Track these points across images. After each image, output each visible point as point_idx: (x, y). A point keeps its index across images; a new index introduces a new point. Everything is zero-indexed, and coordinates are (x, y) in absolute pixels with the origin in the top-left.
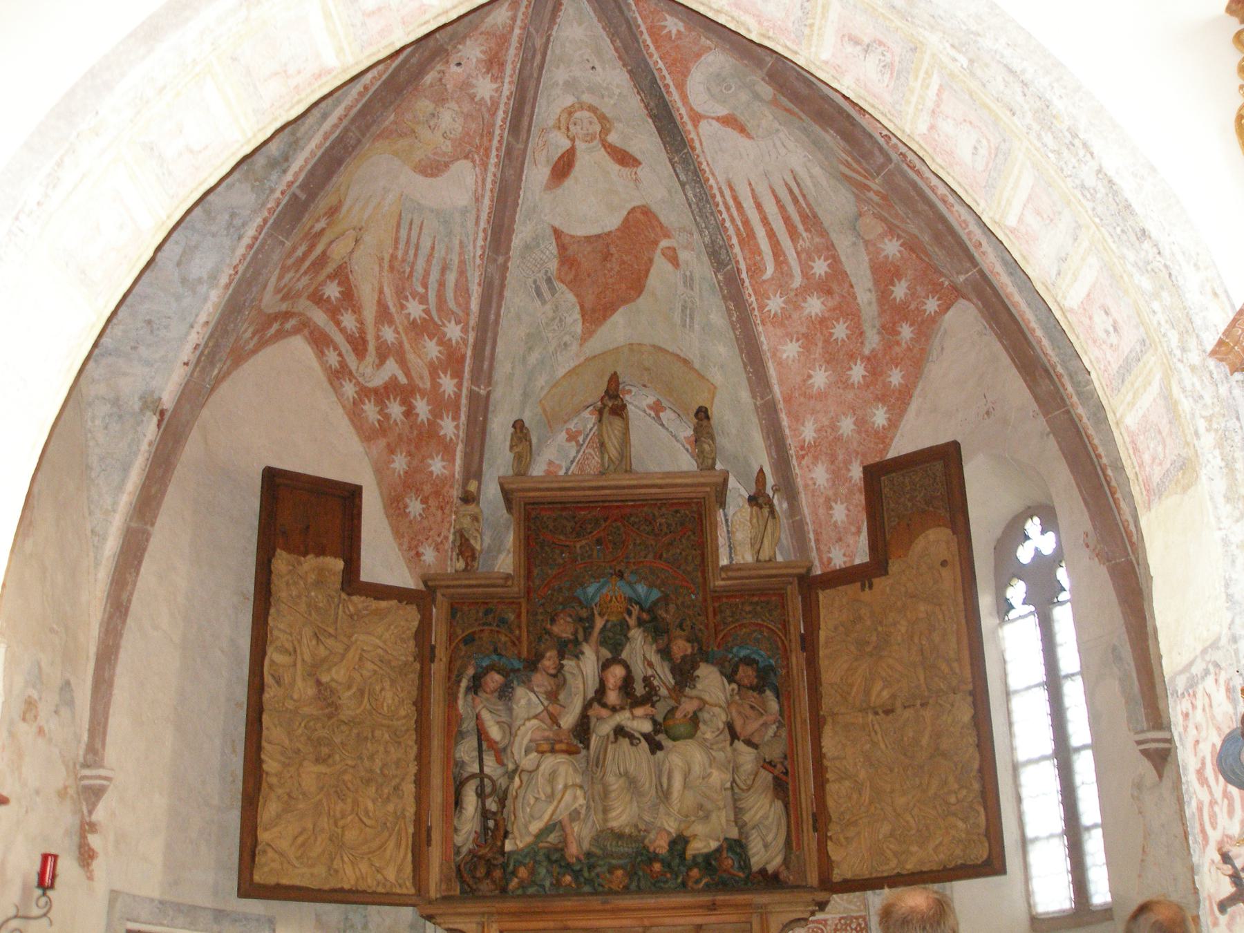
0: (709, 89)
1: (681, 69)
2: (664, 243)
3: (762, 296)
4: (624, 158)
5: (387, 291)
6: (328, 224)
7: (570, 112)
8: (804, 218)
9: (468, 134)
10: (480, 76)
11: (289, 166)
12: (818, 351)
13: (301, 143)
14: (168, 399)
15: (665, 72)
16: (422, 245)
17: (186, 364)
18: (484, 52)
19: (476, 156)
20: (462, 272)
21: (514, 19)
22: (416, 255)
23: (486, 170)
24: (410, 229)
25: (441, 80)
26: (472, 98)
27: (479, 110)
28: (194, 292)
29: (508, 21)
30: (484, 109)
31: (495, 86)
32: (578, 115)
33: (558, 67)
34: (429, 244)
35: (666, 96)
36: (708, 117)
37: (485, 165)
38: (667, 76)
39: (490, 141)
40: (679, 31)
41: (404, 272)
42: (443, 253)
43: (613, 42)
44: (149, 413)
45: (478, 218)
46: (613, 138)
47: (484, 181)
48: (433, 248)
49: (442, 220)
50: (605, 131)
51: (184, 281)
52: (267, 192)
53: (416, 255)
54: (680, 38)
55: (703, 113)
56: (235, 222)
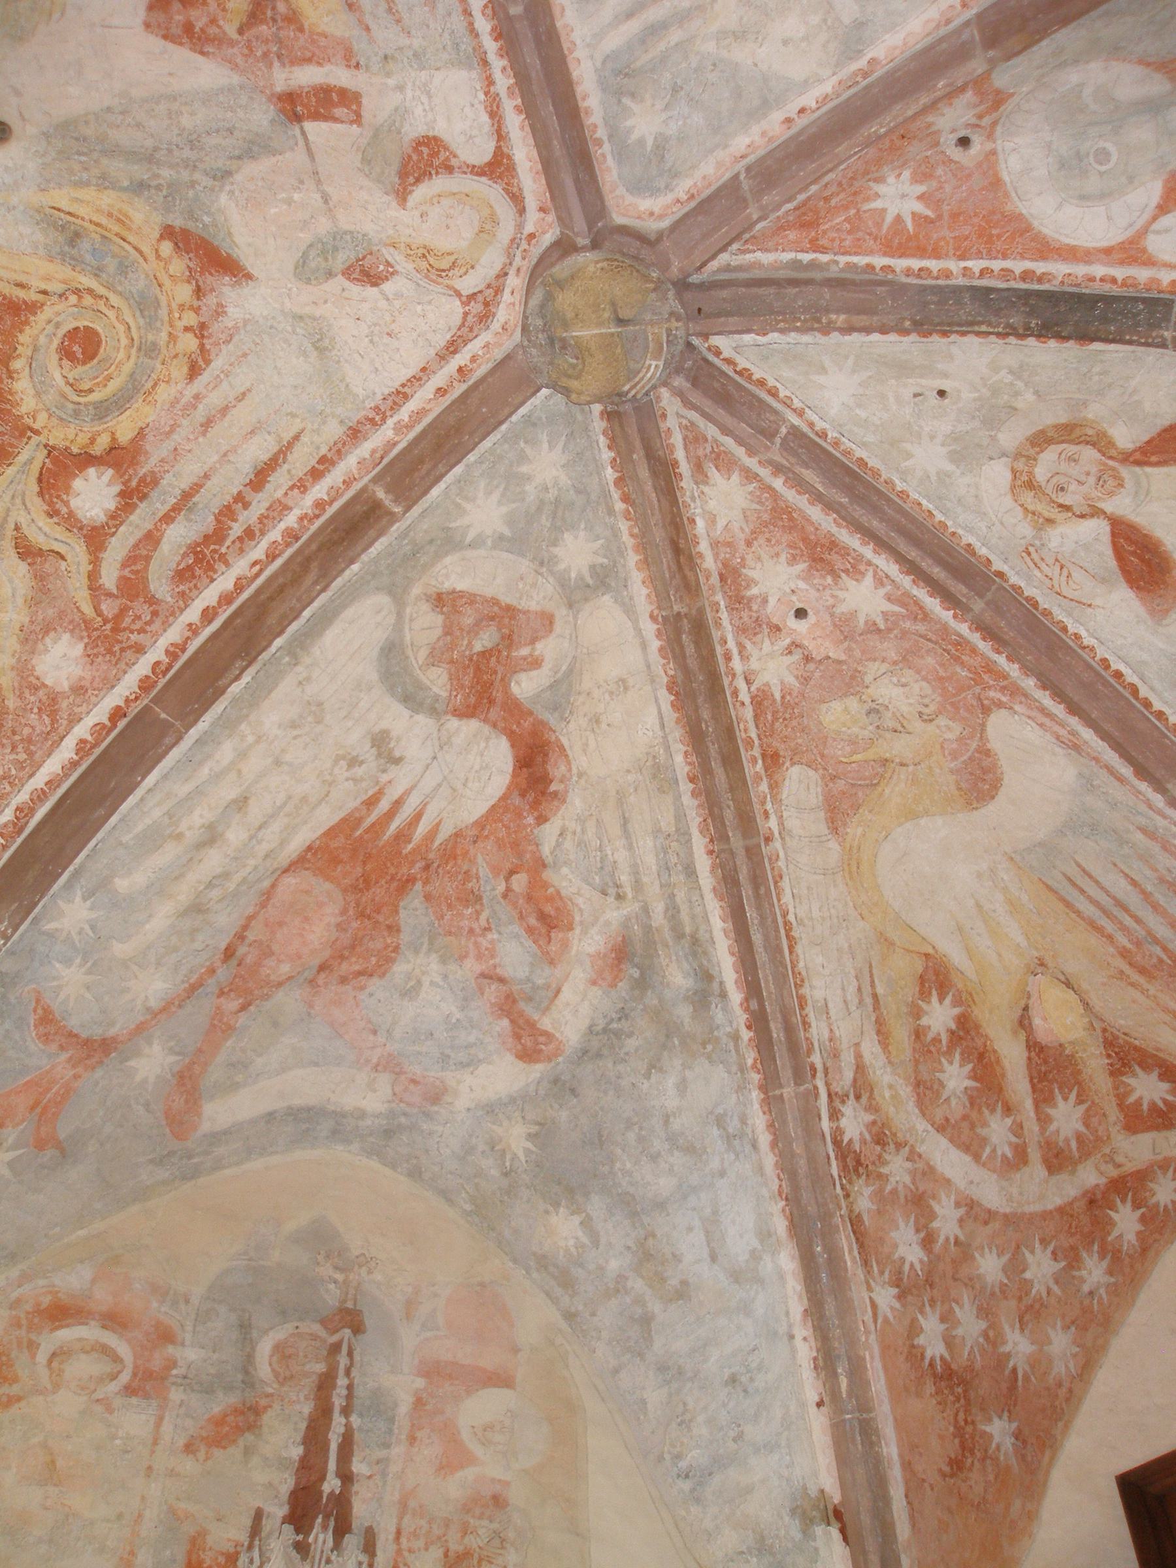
0: (1083, 197)
6: (957, 1002)
7: (1023, 483)
9: (941, 679)
10: (840, 594)
11: (721, 983)
13: (702, 935)
14: (828, 1482)
15: (997, 265)
16: (1120, 895)
17: (820, 1404)
18: (793, 560)
19: (992, 694)
21: (749, 476)
22: (1138, 920)
23: (1026, 695)
24: (1082, 891)
25: (808, 659)
26: (873, 629)
27: (904, 634)
28: (760, 1281)
29: (751, 487)
30: (908, 625)
31: (869, 579)
32: (1041, 473)
33: (909, 455)
34: (1123, 883)
35: (1045, 287)
36: (1144, 232)
37: (1015, 691)
38: (1007, 264)
39: (974, 651)
40: (921, 198)
41: (1161, 961)
42: (1148, 872)
43: (826, 331)
44: (819, 1530)
45: (1111, 771)
46: (1125, 437)
47: (1043, 710)
48: (1134, 883)
49: (1086, 830)
50: (1101, 442)
52: (731, 1046)
53: (1138, 920)
54: (939, 202)
55: (1129, 233)
56: (731, 1130)
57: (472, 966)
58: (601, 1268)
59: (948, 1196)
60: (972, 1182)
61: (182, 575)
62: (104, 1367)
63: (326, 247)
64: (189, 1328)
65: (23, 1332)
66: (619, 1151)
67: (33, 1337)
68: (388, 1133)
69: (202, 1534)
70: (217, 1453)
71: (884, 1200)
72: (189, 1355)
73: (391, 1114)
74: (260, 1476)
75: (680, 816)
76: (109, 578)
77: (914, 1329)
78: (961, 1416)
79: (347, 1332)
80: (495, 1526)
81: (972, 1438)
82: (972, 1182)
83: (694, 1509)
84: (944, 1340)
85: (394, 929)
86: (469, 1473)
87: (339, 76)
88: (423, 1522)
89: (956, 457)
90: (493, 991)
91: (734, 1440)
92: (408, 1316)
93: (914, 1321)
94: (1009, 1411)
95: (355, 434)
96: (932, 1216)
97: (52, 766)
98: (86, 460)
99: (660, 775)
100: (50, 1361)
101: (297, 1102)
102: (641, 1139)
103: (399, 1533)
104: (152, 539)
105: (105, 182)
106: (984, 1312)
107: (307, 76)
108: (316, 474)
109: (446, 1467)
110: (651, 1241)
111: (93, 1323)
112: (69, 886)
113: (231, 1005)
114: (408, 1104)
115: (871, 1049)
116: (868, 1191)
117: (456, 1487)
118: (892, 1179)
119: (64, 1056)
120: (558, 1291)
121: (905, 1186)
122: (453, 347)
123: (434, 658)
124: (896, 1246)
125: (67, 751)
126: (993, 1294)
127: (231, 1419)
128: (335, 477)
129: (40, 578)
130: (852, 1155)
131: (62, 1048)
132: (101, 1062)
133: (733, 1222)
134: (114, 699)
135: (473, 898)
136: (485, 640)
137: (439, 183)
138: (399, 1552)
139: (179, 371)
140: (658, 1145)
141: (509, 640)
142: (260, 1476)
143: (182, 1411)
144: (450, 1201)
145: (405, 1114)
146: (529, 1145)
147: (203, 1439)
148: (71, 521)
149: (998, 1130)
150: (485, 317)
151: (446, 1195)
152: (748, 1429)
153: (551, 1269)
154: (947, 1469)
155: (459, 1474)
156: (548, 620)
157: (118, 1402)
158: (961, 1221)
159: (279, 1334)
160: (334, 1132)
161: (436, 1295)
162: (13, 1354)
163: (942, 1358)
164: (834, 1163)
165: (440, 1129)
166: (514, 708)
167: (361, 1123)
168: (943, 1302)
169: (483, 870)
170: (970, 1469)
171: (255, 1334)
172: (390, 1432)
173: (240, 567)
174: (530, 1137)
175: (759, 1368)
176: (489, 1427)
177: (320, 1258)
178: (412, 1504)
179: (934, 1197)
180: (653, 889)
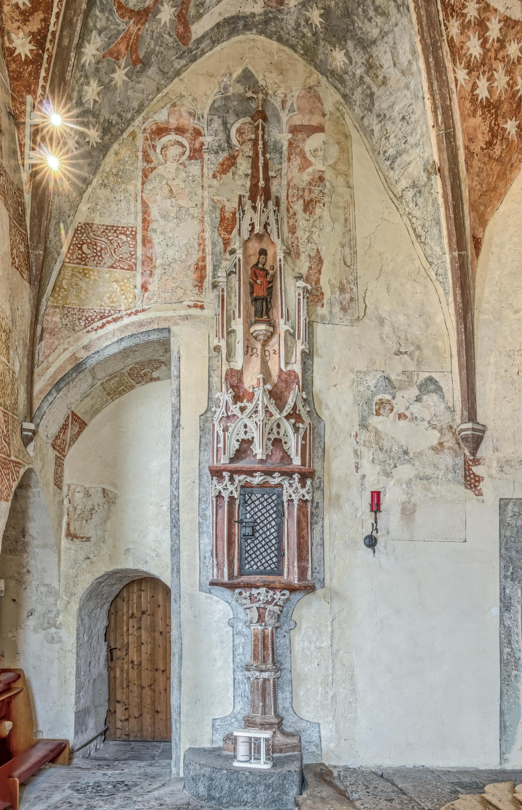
17: (433, 127)
58: (354, 74)
59: (495, 18)
60: (507, 8)
62: (180, 150)
64: (206, 129)
65: (150, 142)
66: (356, 18)
67: (153, 143)
68: (266, 22)
69: (224, 207)
70: (223, 176)
71: (464, 27)
72: (208, 139)
73: (266, 13)
74: (239, 183)
77: (474, 86)
78: (493, 122)
79: (260, 121)
80: (320, 188)
81: (497, 131)
82: (507, 8)
83: (392, 172)
84: (488, 89)
86: (310, 170)
88: (296, 191)
91: (404, 144)
92: (283, 108)
93: (475, 83)
94: (516, 117)
96: (487, 29)
100: (161, 151)
101: (227, 15)
102: (364, 11)
103: (288, 196)
109: (302, 169)
110: (371, 60)
111: (172, 133)
114: (271, 7)
116: (457, 24)
117: (306, 177)
118: (469, 16)
119: (132, 22)
120: (339, 86)
121: (475, 17)
124: (469, 49)
126: (514, 63)
127: (226, 162)
130: (450, 7)
131: (130, 18)
132: (146, 20)
133: (401, 47)
138: (288, 203)
140: (371, 13)
142: (239, 183)
143: (209, 162)
144: (296, 51)
145: (271, 12)
146: (321, 20)
147: (218, 172)
151: (293, 48)
152: (409, 138)
153: (336, 76)
154: (484, 146)
155: (307, 170)
157: (187, 163)
158: (501, 29)
159: (237, 125)
160: (245, 26)
161: (293, 96)
162: (149, 151)
163: (486, 98)
164: (441, 13)
165: (285, 17)
167: (254, 20)
168: (489, 72)
170: (495, 145)
171: (229, 126)
172: (281, 158)
174: (321, 16)
175: (413, 113)
176: (316, 150)
177: (247, 89)
178: (291, 184)
179: (488, 20)
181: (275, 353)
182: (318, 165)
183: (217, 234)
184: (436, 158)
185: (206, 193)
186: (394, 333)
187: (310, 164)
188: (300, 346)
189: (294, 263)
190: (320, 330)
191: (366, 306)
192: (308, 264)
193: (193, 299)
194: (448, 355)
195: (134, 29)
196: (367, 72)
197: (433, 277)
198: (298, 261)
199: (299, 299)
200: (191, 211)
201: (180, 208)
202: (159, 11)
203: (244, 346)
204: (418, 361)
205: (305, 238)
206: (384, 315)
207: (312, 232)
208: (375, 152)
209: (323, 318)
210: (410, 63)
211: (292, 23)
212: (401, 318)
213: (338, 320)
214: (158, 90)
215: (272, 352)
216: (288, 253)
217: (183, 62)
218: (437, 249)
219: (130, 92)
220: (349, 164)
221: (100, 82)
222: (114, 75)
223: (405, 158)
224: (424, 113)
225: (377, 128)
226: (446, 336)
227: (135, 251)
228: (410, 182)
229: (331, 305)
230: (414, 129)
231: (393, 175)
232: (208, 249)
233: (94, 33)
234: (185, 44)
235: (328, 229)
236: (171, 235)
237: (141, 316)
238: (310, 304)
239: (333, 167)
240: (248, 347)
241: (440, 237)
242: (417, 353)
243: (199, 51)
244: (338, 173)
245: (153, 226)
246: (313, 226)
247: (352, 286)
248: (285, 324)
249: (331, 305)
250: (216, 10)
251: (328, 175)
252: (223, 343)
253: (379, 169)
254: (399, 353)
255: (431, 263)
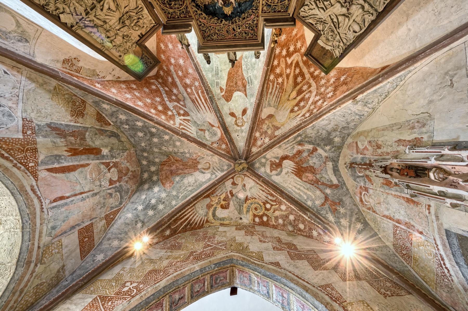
1: (221, 139)
2: (223, 93)
3: (200, 86)
4: (232, 114)
5: (286, 83)
7: (242, 125)
8: (195, 102)
12: (184, 69)
20: (267, 93)
26: (260, 132)
37: (259, 118)
46: (234, 119)
50: (236, 121)
51: (331, 121)
57: (308, 158)
61: (273, 197)
62: (366, 195)
63: (244, 189)
68: (334, 161)
71: (315, 107)
73: (331, 161)
75: (283, 144)
76: (275, 204)
83: (365, 115)
85: (307, 167)
86: (368, 146)
87: (229, 193)
89: (243, 132)
90: (310, 155)
95: (258, 183)
97: (293, 207)
98: (265, 207)
99: (280, 147)
104: (271, 200)
105: (243, 209)
106: (328, 88)
107: (229, 195)
108: (262, 186)
109: (368, 150)
112: (306, 204)
113: (320, 183)
115: (300, 116)
117: (370, 148)
122: (249, 177)
123: (277, 171)
125: (291, 206)
128: (262, 184)
129: (276, 210)
134: (286, 202)
135: (301, 160)
136: (274, 166)
137: (236, 182)
139: (256, 200)
140: (320, 134)
141: (274, 164)
148: (271, 208)
149: (307, 96)
150: (246, 175)
156: (270, 161)
166: (280, 161)
169: (297, 160)
173: (271, 191)
180: (291, 144)
181: (454, 168)
182: (366, 143)
183: (392, 188)
184: (350, 101)
185: (378, 189)
186: (437, 92)
187: (366, 147)
188: (446, 151)
189: (402, 153)
190: (438, 138)
191: (422, 113)
192: (401, 147)
193: (424, 209)
194: (451, 51)
195: (329, 202)
196: (337, 131)
197: (403, 82)
198: (401, 152)
199: (416, 152)
200: (385, 197)
201: (384, 202)
202: (327, 193)
203: (449, 188)
204: (458, 69)
205: (391, 148)
206: (427, 102)
207: (388, 145)
208: (361, 122)
209: (430, 137)
210: (326, 120)
211: (332, 154)
212: (427, 91)
213: (430, 128)
214: (351, 197)
215: (454, 170)
216: (396, 157)
217: (345, 187)
218: (388, 86)
219: (349, 208)
220: (365, 131)
221: (342, 218)
222: (342, 212)
223: (357, 112)
224: (338, 111)
225: (353, 124)
226: (436, 60)
227: (403, 229)
228: (365, 107)
229: (422, 133)
230: (345, 112)
231: (366, 114)
232: (399, 194)
233: (327, 215)
234: (339, 186)
235: (386, 138)
236: (395, 210)
237: (439, 242)
238: (421, 145)
239: (366, 137)
240: (451, 185)
241: (381, 87)
242: (450, 73)
243: (342, 182)
244: (368, 135)
245: (392, 216)
246: (385, 144)
247: (411, 123)
248: (431, 160)
249: (422, 133)
250: (330, 176)
251: (369, 139)
252: (449, 201)
253: (366, 119)
254: (452, 85)
255: (397, 86)
